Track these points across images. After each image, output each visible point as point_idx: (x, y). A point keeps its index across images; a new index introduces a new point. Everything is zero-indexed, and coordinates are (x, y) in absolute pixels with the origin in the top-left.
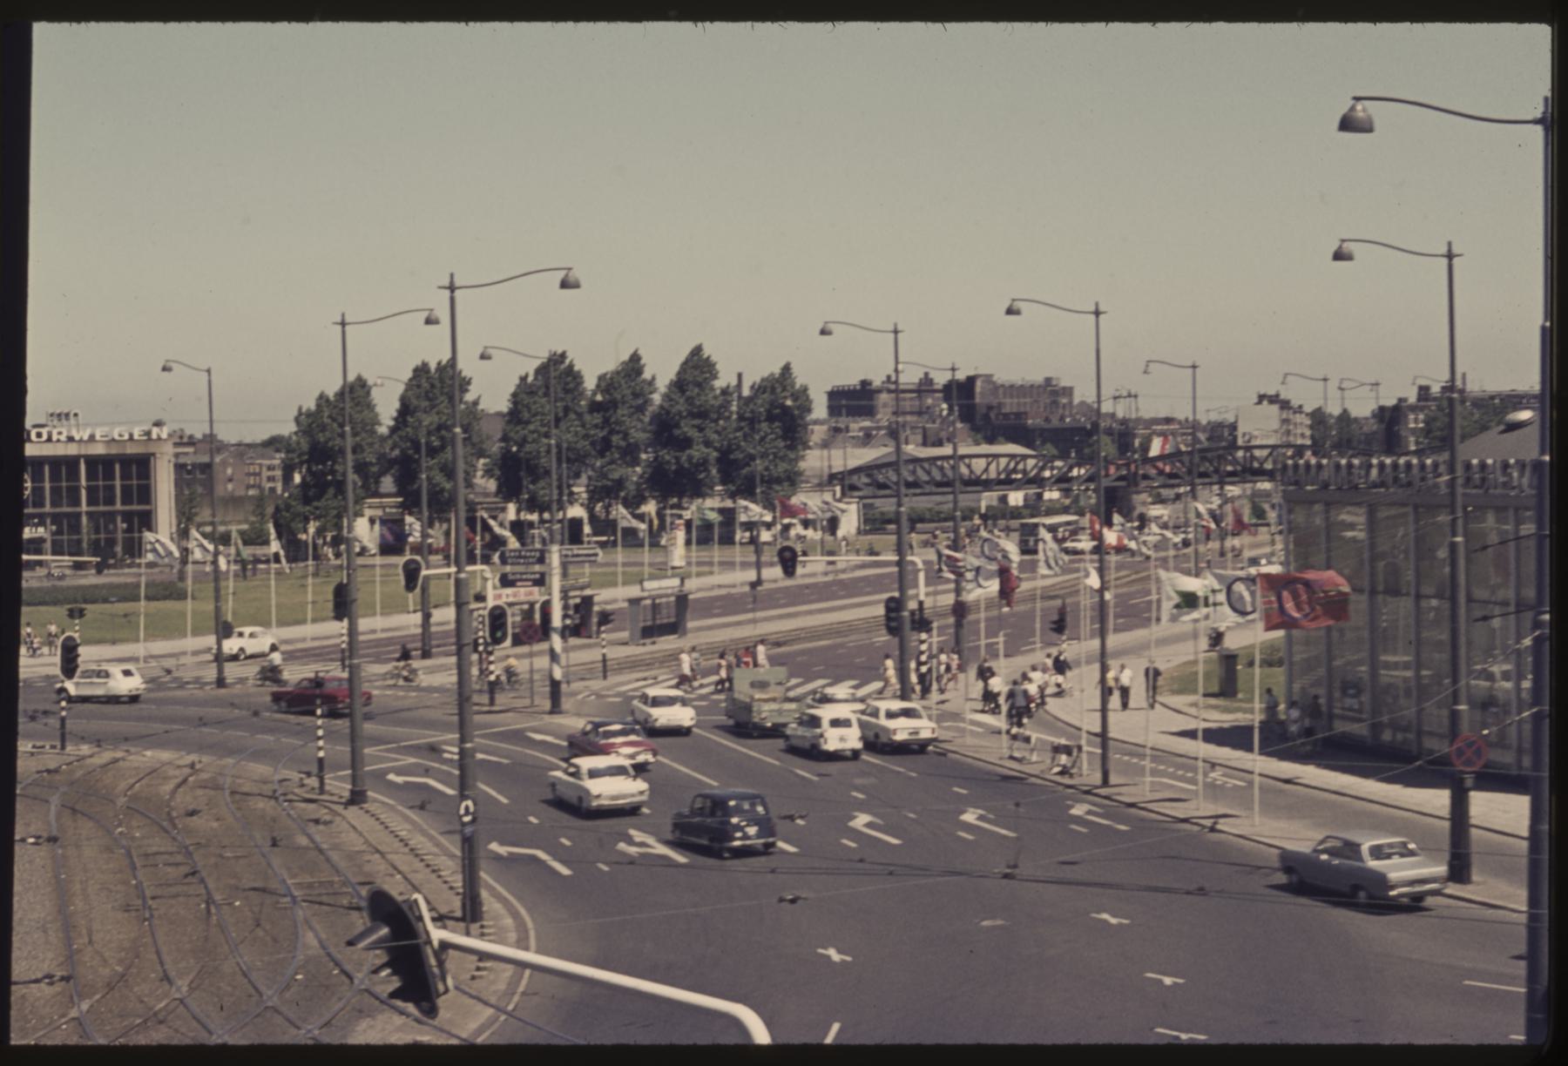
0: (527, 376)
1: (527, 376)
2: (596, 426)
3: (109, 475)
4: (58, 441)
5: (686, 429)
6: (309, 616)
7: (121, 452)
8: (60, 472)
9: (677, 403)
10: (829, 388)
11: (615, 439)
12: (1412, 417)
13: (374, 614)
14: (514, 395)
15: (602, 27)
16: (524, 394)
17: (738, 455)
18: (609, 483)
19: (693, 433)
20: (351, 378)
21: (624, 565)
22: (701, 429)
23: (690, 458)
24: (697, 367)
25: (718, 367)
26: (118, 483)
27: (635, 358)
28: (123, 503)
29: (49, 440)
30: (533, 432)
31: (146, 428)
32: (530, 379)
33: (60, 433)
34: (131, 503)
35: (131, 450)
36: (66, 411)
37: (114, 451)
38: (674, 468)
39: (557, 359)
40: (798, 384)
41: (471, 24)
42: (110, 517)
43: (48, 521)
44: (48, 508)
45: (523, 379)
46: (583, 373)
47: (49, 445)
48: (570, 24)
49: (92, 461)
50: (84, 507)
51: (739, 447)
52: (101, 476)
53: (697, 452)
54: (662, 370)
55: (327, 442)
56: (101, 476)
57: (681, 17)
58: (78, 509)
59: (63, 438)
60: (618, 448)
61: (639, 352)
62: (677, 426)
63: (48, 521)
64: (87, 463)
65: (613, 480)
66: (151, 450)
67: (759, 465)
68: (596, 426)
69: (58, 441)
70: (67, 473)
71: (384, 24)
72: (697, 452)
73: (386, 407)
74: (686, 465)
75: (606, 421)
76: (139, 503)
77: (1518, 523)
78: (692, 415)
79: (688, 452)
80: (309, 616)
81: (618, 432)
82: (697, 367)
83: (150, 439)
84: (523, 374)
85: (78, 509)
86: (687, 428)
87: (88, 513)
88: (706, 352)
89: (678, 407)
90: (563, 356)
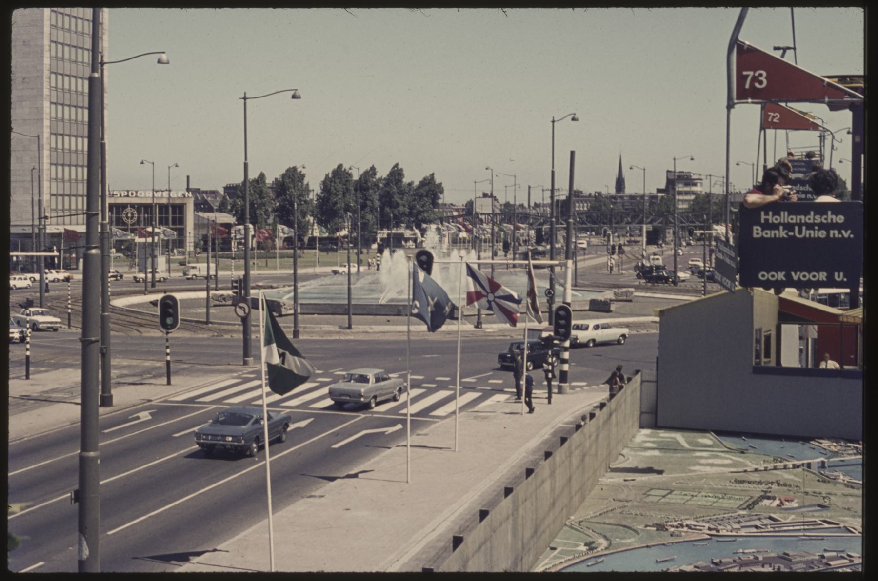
10: (225, 185)
11: (368, 203)
12: (577, 205)
14: (324, 183)
15: (517, 10)
16: (327, 185)
20: (253, 175)
23: (399, 211)
24: (396, 174)
27: (373, 166)
29: (136, 196)
31: (183, 192)
32: (330, 176)
34: (176, 225)
35: (177, 202)
40: (437, 182)
41: (576, 10)
45: (327, 176)
46: (404, 172)
47: (121, 199)
48: (556, 9)
49: (161, 206)
54: (383, 172)
57: (406, 7)
61: (375, 166)
66: (185, 202)
71: (806, 9)
72: (401, 208)
76: (179, 224)
77: (71, 254)
81: (369, 200)
82: (396, 174)
83: (185, 197)
86: (397, 198)
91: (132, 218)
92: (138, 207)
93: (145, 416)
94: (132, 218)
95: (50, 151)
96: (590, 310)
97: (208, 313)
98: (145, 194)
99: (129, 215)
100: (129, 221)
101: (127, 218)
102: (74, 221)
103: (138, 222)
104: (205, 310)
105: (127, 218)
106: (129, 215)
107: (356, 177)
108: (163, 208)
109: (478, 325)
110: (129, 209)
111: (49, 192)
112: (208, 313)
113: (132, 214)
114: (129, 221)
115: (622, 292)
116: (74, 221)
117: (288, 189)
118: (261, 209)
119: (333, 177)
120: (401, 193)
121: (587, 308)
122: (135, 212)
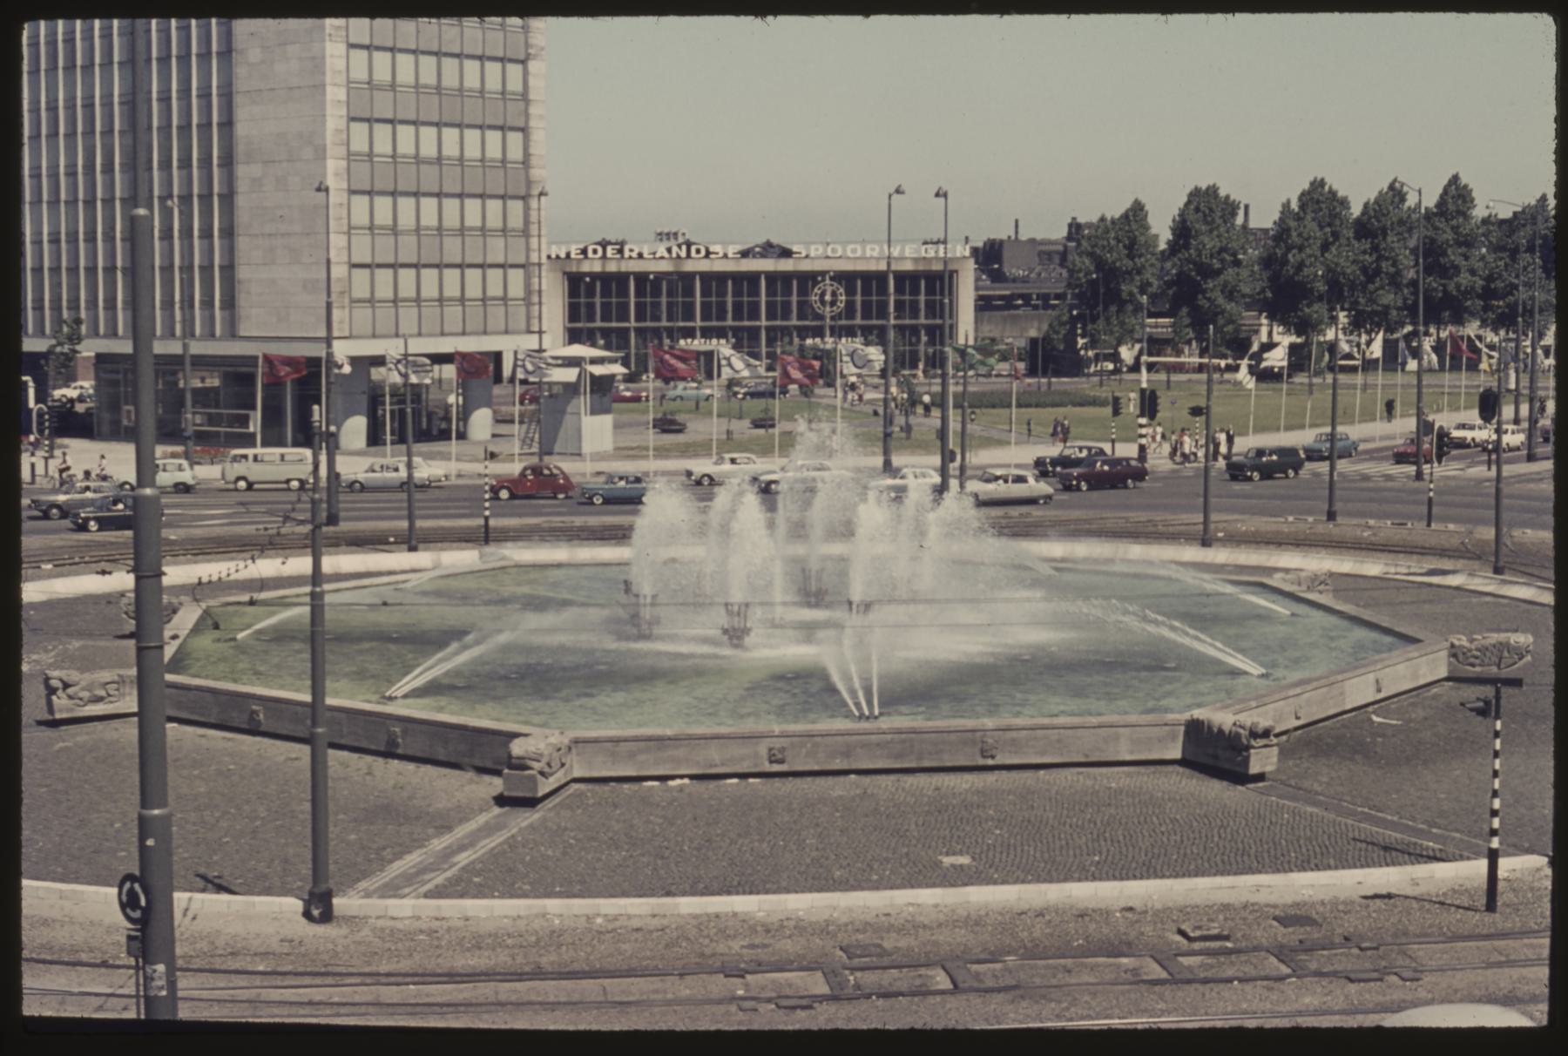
0: (1289, 202)
1: (1289, 202)
2: (1364, 252)
3: (722, 293)
4: (630, 258)
5: (1452, 258)
6: (1308, 421)
7: (927, 268)
8: (726, 287)
9: (1445, 232)
12: (667, 341)
13: (1375, 420)
17: (1500, 284)
18: (1380, 308)
19: (1460, 261)
21: (1466, 387)
22: (1466, 258)
23: (1458, 286)
24: (1456, 196)
25: (1474, 194)
26: (922, 298)
28: (863, 318)
29: (708, 254)
30: (1310, 256)
32: (1294, 206)
33: (631, 250)
36: (674, 230)
37: (921, 268)
38: (1440, 295)
39: (1318, 184)
42: (915, 330)
43: (730, 334)
44: (699, 323)
49: (901, 277)
50: (892, 322)
51: (1500, 276)
52: (614, 294)
53: (1464, 279)
55: (1114, 262)
56: (614, 294)
58: (758, 323)
59: (634, 255)
60: (1387, 274)
62: (1444, 254)
63: (730, 334)
64: (767, 278)
65: (1383, 306)
67: (1522, 294)
68: (1364, 252)
69: (630, 258)
70: (602, 290)
72: (1464, 279)
73: (1161, 229)
74: (1454, 293)
75: (1375, 248)
76: (618, 320)
78: (1459, 244)
79: (1455, 279)
80: (1308, 421)
81: (1387, 259)
82: (1456, 196)
84: (1284, 200)
85: (758, 323)
86: (1454, 256)
87: (895, 326)
88: (1464, 180)
89: (1445, 236)
90: (1322, 183)
91: (833, 303)
92: (846, 279)
93: (599, 920)
94: (833, 303)
95: (349, 161)
96: (1182, 762)
97: (1206, 522)
98: (864, 251)
99: (828, 298)
100: (828, 309)
101: (823, 302)
102: (474, 322)
103: (850, 310)
104: (1200, 518)
105: (823, 302)
106: (828, 298)
107: (1356, 210)
108: (907, 280)
109: (319, 906)
110: (828, 286)
111: (345, 259)
112: (1206, 522)
113: (834, 294)
114: (828, 309)
115: (1483, 650)
116: (453, 323)
117: (1195, 238)
118: (1132, 280)
119: (1302, 207)
120: (1467, 243)
121: (1176, 753)
122: (842, 290)
